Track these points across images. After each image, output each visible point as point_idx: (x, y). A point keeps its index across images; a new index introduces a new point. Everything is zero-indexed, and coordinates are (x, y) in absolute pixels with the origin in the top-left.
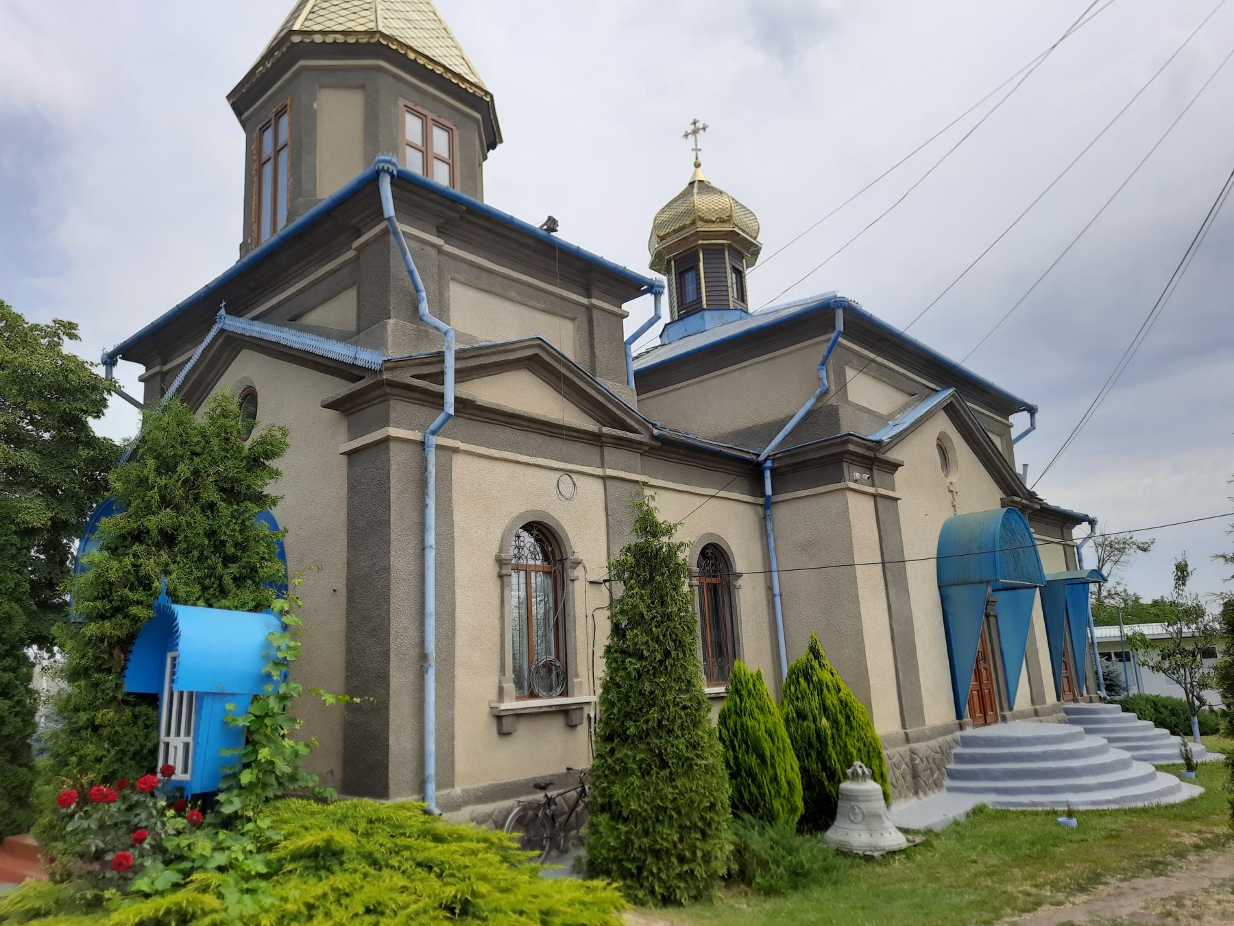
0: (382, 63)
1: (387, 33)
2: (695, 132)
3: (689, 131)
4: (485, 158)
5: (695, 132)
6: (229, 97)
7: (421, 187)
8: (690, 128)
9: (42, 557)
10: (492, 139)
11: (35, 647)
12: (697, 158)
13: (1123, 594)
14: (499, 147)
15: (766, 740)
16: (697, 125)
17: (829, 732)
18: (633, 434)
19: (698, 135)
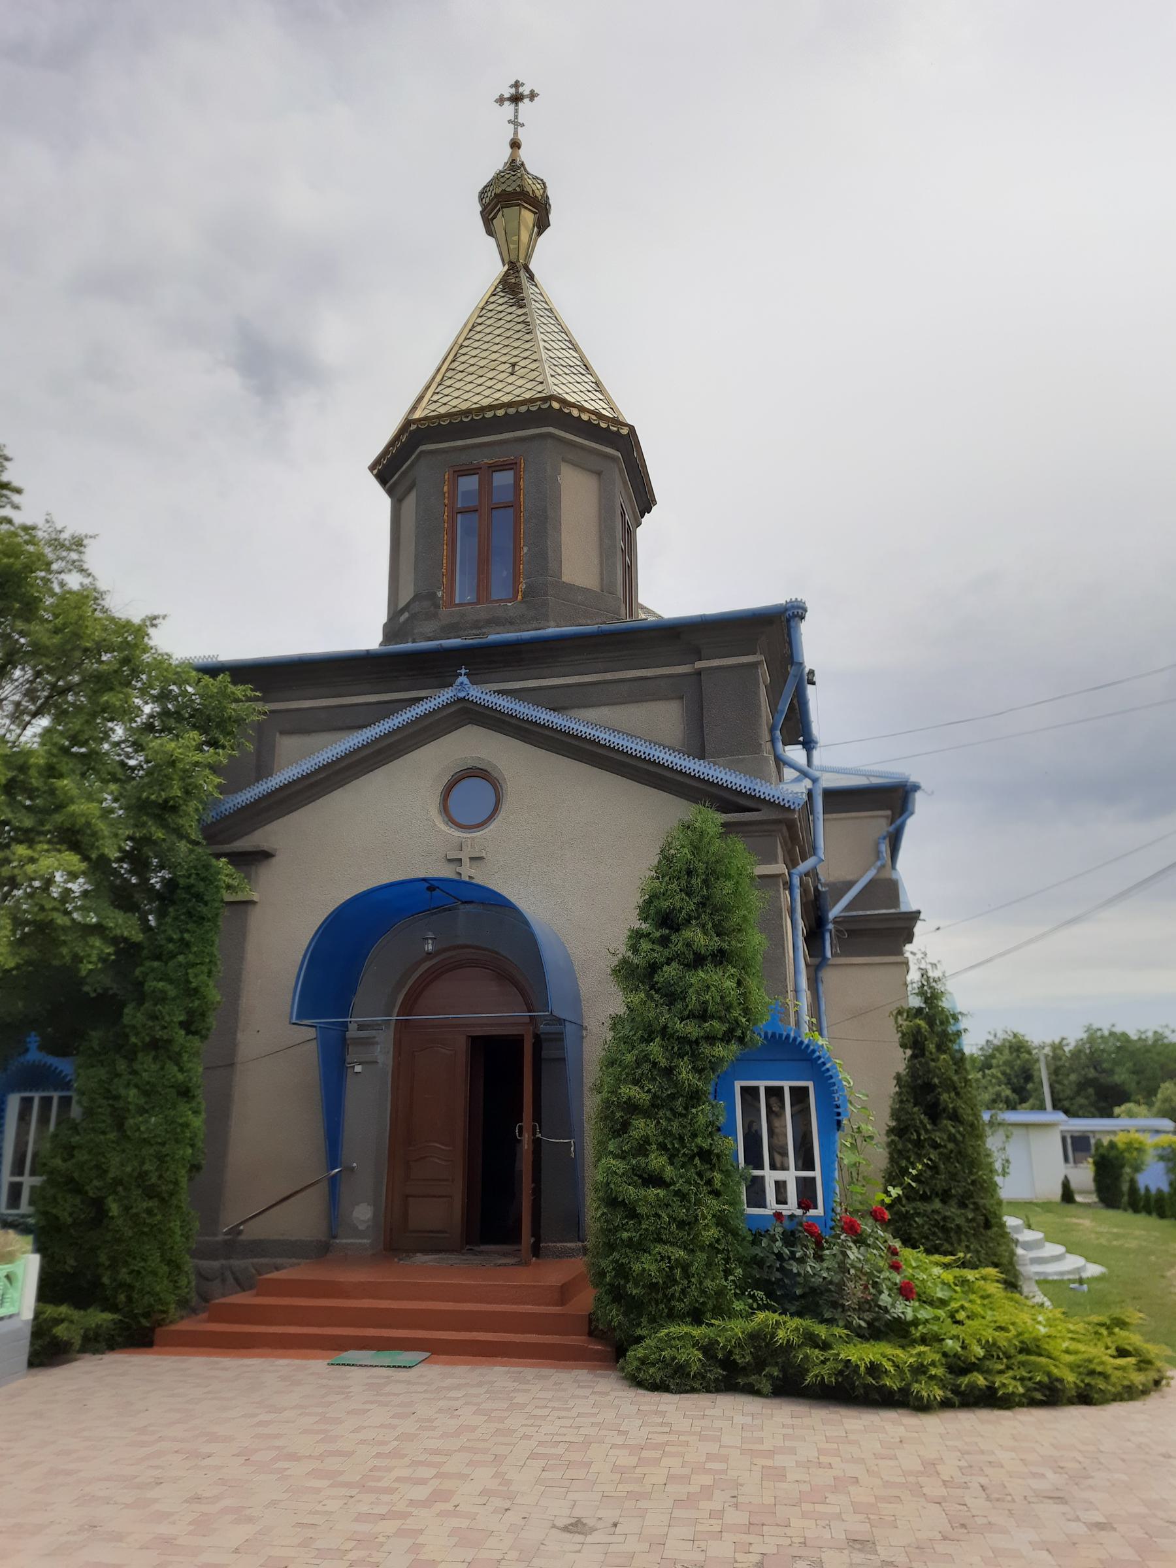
0: (551, 430)
1: (572, 400)
2: (516, 99)
3: (507, 95)
4: (639, 524)
5: (516, 99)
6: (372, 468)
7: (1130, 890)
8: (508, 92)
9: (63, 938)
10: (645, 501)
11: (38, 1039)
12: (515, 145)
13: (168, 1136)
14: (654, 509)
15: (1117, 1236)
16: (521, 89)
17: (938, 1289)
18: (324, 704)
19: (520, 104)
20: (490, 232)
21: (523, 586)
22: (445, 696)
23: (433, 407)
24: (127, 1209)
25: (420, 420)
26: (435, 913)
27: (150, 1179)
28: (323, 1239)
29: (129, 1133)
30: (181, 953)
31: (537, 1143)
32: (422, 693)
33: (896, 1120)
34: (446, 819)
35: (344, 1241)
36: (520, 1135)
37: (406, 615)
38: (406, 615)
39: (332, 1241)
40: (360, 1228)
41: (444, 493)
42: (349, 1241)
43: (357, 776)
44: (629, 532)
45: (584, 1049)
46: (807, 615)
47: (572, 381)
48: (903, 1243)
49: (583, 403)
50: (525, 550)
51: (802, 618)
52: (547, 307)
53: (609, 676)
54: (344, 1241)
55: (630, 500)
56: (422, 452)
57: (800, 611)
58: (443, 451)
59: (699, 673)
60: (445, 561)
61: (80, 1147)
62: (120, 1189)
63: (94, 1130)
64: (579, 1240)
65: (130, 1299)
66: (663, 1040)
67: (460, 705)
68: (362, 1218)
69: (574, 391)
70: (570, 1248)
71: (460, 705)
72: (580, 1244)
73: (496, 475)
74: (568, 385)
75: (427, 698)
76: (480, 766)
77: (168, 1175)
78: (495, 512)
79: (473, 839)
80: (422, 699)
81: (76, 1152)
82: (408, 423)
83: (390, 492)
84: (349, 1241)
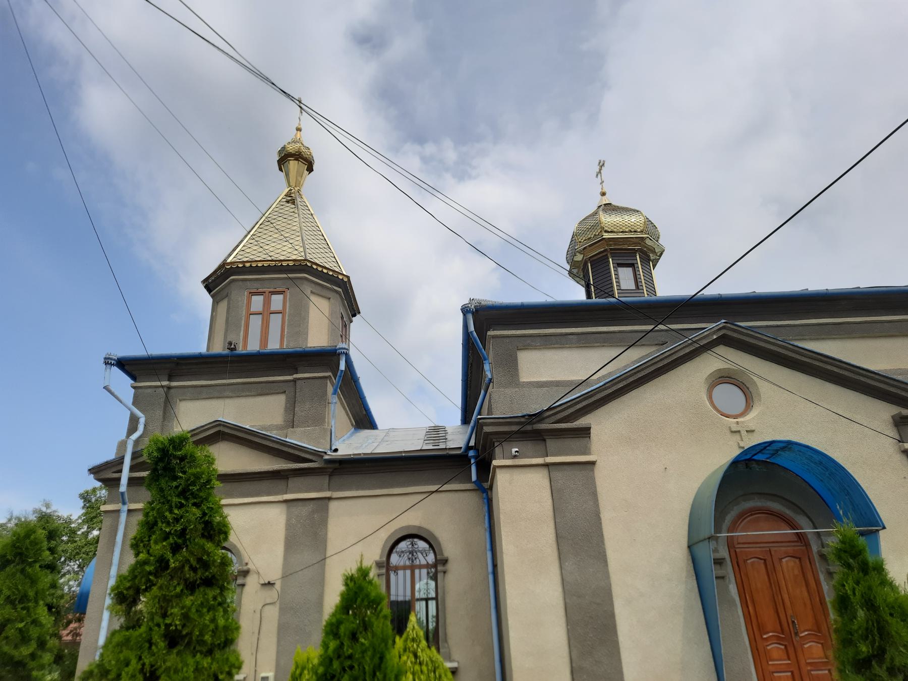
4: (351, 322)
6: (204, 281)
20: (281, 169)
23: (240, 257)
25: (231, 263)
33: (374, 600)
41: (96, 648)
44: (346, 326)
45: (380, 551)
47: (316, 257)
48: (334, 637)
49: (324, 263)
52: (310, 213)
55: (346, 310)
56: (234, 280)
66: (15, 632)
69: (319, 258)
73: (273, 296)
74: (328, 263)
78: (271, 315)
82: (223, 265)
83: (212, 296)
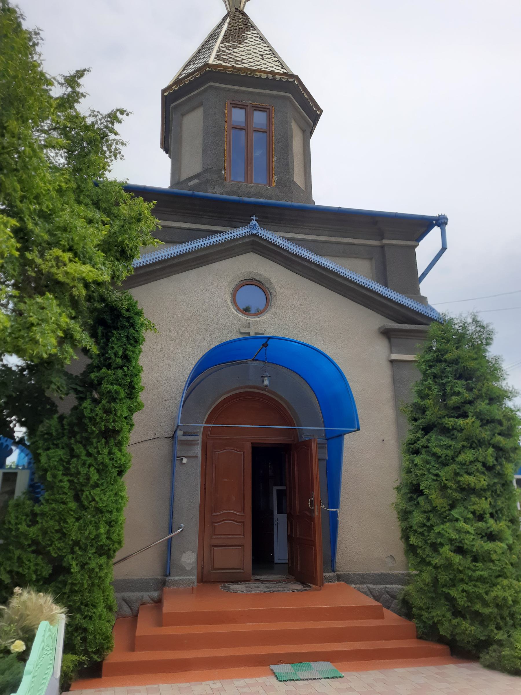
21: (275, 179)
22: (241, 231)
24: (83, 566)
26: (233, 365)
27: (101, 540)
28: (159, 577)
29: (86, 503)
30: (92, 372)
31: (243, 511)
32: (219, 229)
34: (236, 308)
35: (177, 578)
36: (312, 505)
37: (196, 181)
38: (196, 181)
39: (167, 578)
40: (187, 569)
42: (181, 578)
43: (177, 272)
46: (448, 223)
50: (275, 158)
51: (446, 224)
53: (333, 239)
54: (177, 578)
56: (211, 86)
57: (446, 221)
58: (228, 90)
59: (382, 247)
60: (226, 154)
61: (43, 514)
62: (77, 549)
63: (56, 501)
64: (333, 571)
65: (84, 640)
67: (251, 239)
68: (188, 562)
70: (330, 577)
71: (251, 239)
72: (335, 574)
75: (223, 232)
76: (257, 279)
77: (115, 537)
79: (256, 322)
80: (220, 232)
81: (38, 519)
84: (181, 578)
